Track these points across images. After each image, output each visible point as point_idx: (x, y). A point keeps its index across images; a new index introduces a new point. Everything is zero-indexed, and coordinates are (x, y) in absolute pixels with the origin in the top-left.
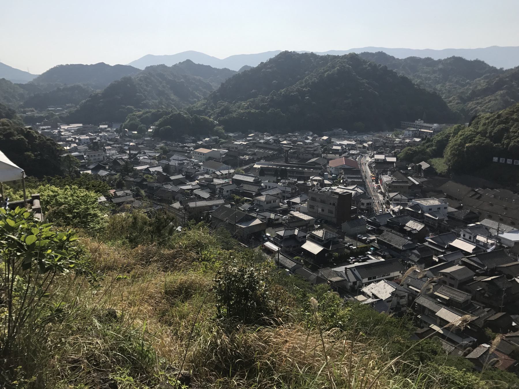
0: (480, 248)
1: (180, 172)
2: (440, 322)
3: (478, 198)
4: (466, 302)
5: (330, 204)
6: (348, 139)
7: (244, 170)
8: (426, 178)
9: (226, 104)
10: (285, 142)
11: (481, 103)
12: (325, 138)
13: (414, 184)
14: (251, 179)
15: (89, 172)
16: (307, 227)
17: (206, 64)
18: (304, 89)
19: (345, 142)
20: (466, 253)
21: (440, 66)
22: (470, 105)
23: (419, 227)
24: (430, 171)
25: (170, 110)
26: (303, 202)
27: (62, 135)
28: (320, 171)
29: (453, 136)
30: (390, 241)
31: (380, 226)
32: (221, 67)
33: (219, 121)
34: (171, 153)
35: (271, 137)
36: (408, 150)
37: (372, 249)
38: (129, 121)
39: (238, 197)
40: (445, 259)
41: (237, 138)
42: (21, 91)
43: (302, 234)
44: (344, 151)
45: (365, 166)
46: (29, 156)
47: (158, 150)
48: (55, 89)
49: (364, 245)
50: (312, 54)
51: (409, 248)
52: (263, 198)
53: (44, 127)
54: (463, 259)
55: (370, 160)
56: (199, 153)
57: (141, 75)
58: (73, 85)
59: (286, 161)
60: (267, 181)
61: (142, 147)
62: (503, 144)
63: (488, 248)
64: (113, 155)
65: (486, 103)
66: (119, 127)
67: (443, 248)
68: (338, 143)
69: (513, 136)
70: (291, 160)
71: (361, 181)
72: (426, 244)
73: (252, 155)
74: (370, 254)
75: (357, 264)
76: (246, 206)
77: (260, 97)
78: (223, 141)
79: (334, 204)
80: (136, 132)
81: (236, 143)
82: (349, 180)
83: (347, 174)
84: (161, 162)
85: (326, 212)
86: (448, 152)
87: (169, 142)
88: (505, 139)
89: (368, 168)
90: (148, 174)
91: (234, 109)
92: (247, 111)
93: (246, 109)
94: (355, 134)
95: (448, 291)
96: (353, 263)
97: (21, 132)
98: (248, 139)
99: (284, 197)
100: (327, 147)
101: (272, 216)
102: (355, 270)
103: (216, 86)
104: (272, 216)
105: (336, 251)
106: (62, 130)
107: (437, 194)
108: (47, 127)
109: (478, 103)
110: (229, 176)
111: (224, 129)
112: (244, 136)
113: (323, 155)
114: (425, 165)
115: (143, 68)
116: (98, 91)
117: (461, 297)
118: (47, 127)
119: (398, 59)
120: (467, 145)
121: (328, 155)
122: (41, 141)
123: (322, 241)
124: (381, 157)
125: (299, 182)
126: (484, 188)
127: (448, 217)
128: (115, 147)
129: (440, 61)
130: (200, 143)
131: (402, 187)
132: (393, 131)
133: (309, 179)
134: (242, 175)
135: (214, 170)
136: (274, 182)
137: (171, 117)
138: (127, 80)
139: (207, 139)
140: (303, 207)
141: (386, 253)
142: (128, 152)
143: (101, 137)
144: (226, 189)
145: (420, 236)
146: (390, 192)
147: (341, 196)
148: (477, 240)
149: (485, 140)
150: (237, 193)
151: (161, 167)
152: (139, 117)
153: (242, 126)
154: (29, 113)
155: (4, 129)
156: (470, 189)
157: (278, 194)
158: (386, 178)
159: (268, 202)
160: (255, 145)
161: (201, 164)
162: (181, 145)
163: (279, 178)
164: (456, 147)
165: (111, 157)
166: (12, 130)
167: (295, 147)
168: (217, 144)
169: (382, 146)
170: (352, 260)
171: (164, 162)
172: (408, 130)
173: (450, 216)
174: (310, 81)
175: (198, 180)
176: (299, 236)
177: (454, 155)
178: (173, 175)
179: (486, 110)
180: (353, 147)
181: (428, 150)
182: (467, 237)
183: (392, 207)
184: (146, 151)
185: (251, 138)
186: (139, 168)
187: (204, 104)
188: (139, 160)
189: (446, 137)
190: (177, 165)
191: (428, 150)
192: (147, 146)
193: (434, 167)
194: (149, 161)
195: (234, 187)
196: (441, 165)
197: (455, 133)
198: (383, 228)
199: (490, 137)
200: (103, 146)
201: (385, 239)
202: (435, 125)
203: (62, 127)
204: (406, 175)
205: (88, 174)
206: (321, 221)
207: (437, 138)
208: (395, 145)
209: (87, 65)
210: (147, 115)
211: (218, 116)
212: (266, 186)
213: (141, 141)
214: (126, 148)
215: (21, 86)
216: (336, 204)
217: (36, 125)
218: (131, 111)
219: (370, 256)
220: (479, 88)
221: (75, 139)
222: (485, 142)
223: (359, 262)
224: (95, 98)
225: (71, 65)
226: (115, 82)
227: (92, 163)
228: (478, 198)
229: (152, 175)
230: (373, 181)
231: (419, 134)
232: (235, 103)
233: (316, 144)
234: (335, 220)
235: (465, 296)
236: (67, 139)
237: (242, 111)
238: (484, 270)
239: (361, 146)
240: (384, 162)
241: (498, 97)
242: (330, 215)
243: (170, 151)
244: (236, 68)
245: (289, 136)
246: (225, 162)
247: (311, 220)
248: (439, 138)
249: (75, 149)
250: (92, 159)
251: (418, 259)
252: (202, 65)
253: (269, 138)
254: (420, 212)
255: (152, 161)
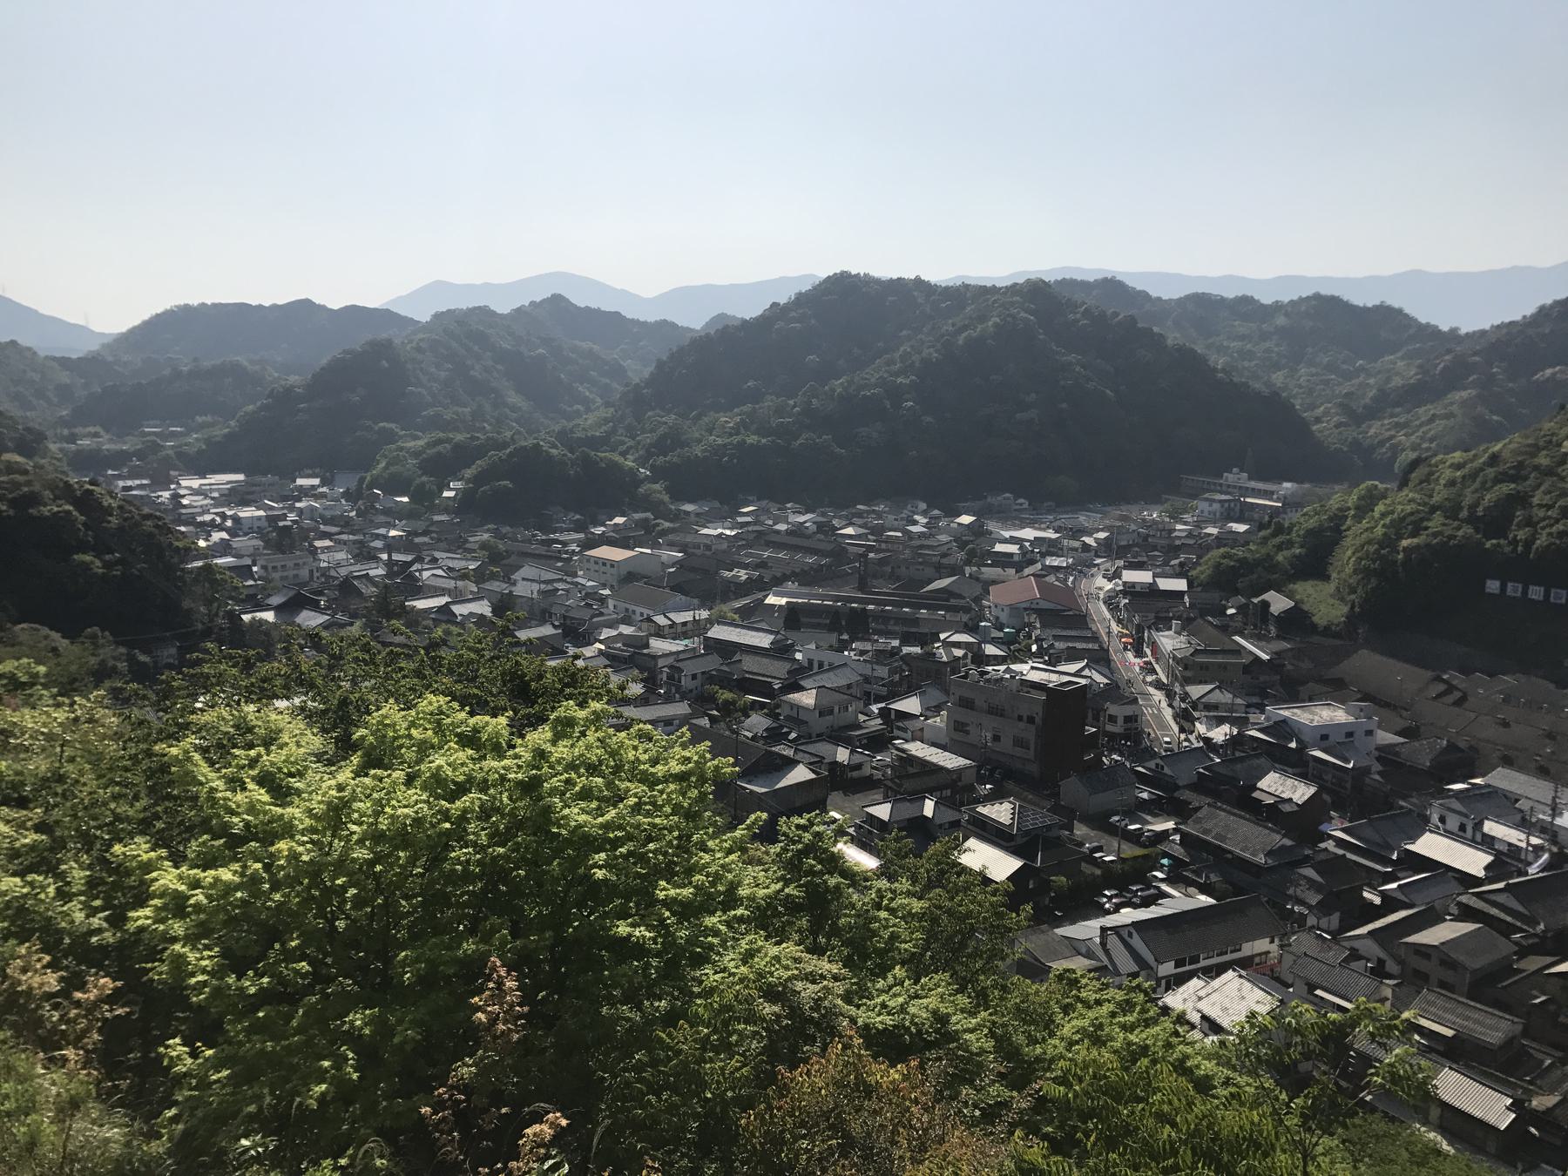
0: (1505, 861)
1: (543, 617)
2: (1441, 1117)
3: (1459, 703)
4: (1509, 1042)
5: (1020, 718)
6: (1032, 524)
7: (737, 611)
8: (1284, 639)
9: (671, 419)
10: (850, 531)
11: (1405, 425)
12: (966, 519)
13: (1257, 658)
14: (763, 640)
15: (269, 616)
16: (953, 789)
17: (607, 307)
18: (899, 380)
19: (1028, 534)
20: (1466, 880)
21: (1281, 321)
22: (1372, 431)
23: (1300, 792)
24: (1296, 621)
25: (508, 434)
26: (931, 710)
27: (185, 507)
28: (965, 618)
29: (1358, 518)
30: (1223, 839)
31: (1177, 788)
32: (651, 317)
33: (653, 468)
34: (512, 560)
35: (809, 516)
36: (1224, 557)
37: (1165, 861)
38: (386, 468)
39: (726, 695)
40: (1403, 898)
41: (707, 519)
42: (64, 377)
43: (950, 815)
44: (1026, 559)
45: (1096, 604)
46: (86, 567)
47: (474, 551)
48: (167, 372)
49: (1139, 852)
50: (918, 281)
51: (1287, 862)
52: (807, 699)
53: (129, 483)
54: (1464, 899)
55: (1109, 586)
56: (597, 560)
57: (421, 336)
58: (218, 362)
59: (862, 587)
60: (813, 646)
61: (425, 544)
62: (1515, 542)
63: (1530, 864)
64: (338, 565)
65: (1421, 425)
66: (353, 485)
67: (1386, 861)
68: (1007, 534)
69: (1544, 519)
70: (875, 582)
71: (1096, 647)
72: (1330, 845)
73: (757, 567)
74: (1162, 880)
75: (1128, 915)
76: (757, 723)
77: (769, 402)
78: (667, 525)
79: (1031, 720)
80: (406, 499)
81: (705, 531)
82: (1060, 645)
83: (1053, 626)
84: (487, 586)
85: (1006, 745)
86: (1346, 560)
87: (506, 529)
88: (1520, 526)
89: (1104, 608)
90: (448, 622)
91: (697, 435)
92: (736, 439)
93: (731, 435)
94: (1049, 512)
95: (1446, 1010)
96: (1117, 909)
97: (66, 492)
98: (740, 519)
99: (868, 694)
100: (975, 546)
101: (842, 755)
102: (1130, 935)
103: (639, 371)
104: (842, 755)
105: (1059, 869)
106: (182, 492)
107: (1336, 690)
108: (138, 482)
109: (1398, 426)
110: (697, 628)
111: (667, 490)
112: (728, 513)
113: (968, 570)
114: (1279, 603)
115: (424, 317)
116: (293, 379)
117: (1493, 1029)
118: (138, 482)
119: (1159, 299)
120: (1405, 543)
121: (983, 569)
122: (125, 520)
123: (1011, 837)
124: (1143, 577)
125: (906, 650)
126: (1466, 671)
127: (1378, 759)
128: (345, 543)
129: (1277, 307)
130: (599, 530)
131: (1224, 667)
132: (1162, 503)
133: (938, 640)
134: (737, 626)
135: (646, 612)
136: (831, 648)
137: (511, 455)
138: (381, 349)
139: (619, 520)
140: (932, 727)
141: (1214, 878)
142: (385, 556)
143: (301, 512)
144: (689, 668)
145: (1301, 824)
146: (1188, 681)
147: (1055, 695)
148: (1484, 835)
149: (1458, 528)
150: (724, 681)
151: (486, 602)
152: (416, 454)
153: (721, 483)
154: (85, 442)
155: (13, 482)
156: (1430, 674)
157: (849, 686)
158: (1170, 641)
159: (823, 711)
160: (764, 538)
161: (607, 592)
162: (541, 536)
163: (845, 637)
164: (1372, 549)
165: (333, 573)
166: (37, 487)
167: (883, 546)
168: (644, 534)
169: (1137, 545)
170: (1109, 898)
171: (497, 586)
172: (1207, 499)
173: (1386, 755)
174: (916, 358)
175: (601, 642)
176: (938, 822)
177: (1365, 573)
178: (524, 625)
179: (1425, 445)
180: (1052, 548)
181: (1280, 558)
182: (1453, 823)
183: (1201, 728)
184: (437, 554)
185: (749, 519)
186: (421, 604)
187: (606, 421)
188: (417, 580)
189: (1331, 519)
190: (535, 595)
191: (1280, 558)
192: (439, 540)
193: (1305, 607)
194: (451, 584)
195: (713, 663)
196: (1325, 602)
197: (1364, 508)
198: (1186, 795)
199: (1472, 520)
200: (306, 538)
201: (1206, 832)
202: (1287, 485)
203: (184, 483)
204: (1226, 629)
205: (262, 622)
206: (992, 772)
207: (1304, 521)
208: (1178, 542)
209: (260, 306)
210: (440, 448)
211: (649, 455)
212: (811, 662)
213: (420, 525)
214: (378, 544)
215: (65, 363)
216: (1038, 720)
217: (106, 476)
218: (391, 437)
219: (1165, 887)
220: (1397, 382)
221: (224, 516)
222: (1460, 533)
223: (1135, 906)
224: (285, 398)
225: (215, 305)
226: (344, 352)
227: (277, 591)
228: (1459, 703)
229: (462, 625)
230: (1125, 649)
231: (1241, 511)
232: (699, 417)
233: (944, 538)
234: (1034, 769)
235: (1505, 1025)
236: (199, 519)
237: (720, 441)
238: (1536, 935)
239: (1076, 544)
240: (1152, 591)
241: (1454, 408)
242: (1019, 752)
243: (509, 553)
244: (695, 320)
245: (860, 515)
246: (677, 588)
247: (966, 768)
248: (1312, 523)
249: (224, 548)
250: (277, 576)
251: (1320, 897)
252: (598, 311)
253: (801, 519)
254: (1293, 745)
255: (460, 583)
